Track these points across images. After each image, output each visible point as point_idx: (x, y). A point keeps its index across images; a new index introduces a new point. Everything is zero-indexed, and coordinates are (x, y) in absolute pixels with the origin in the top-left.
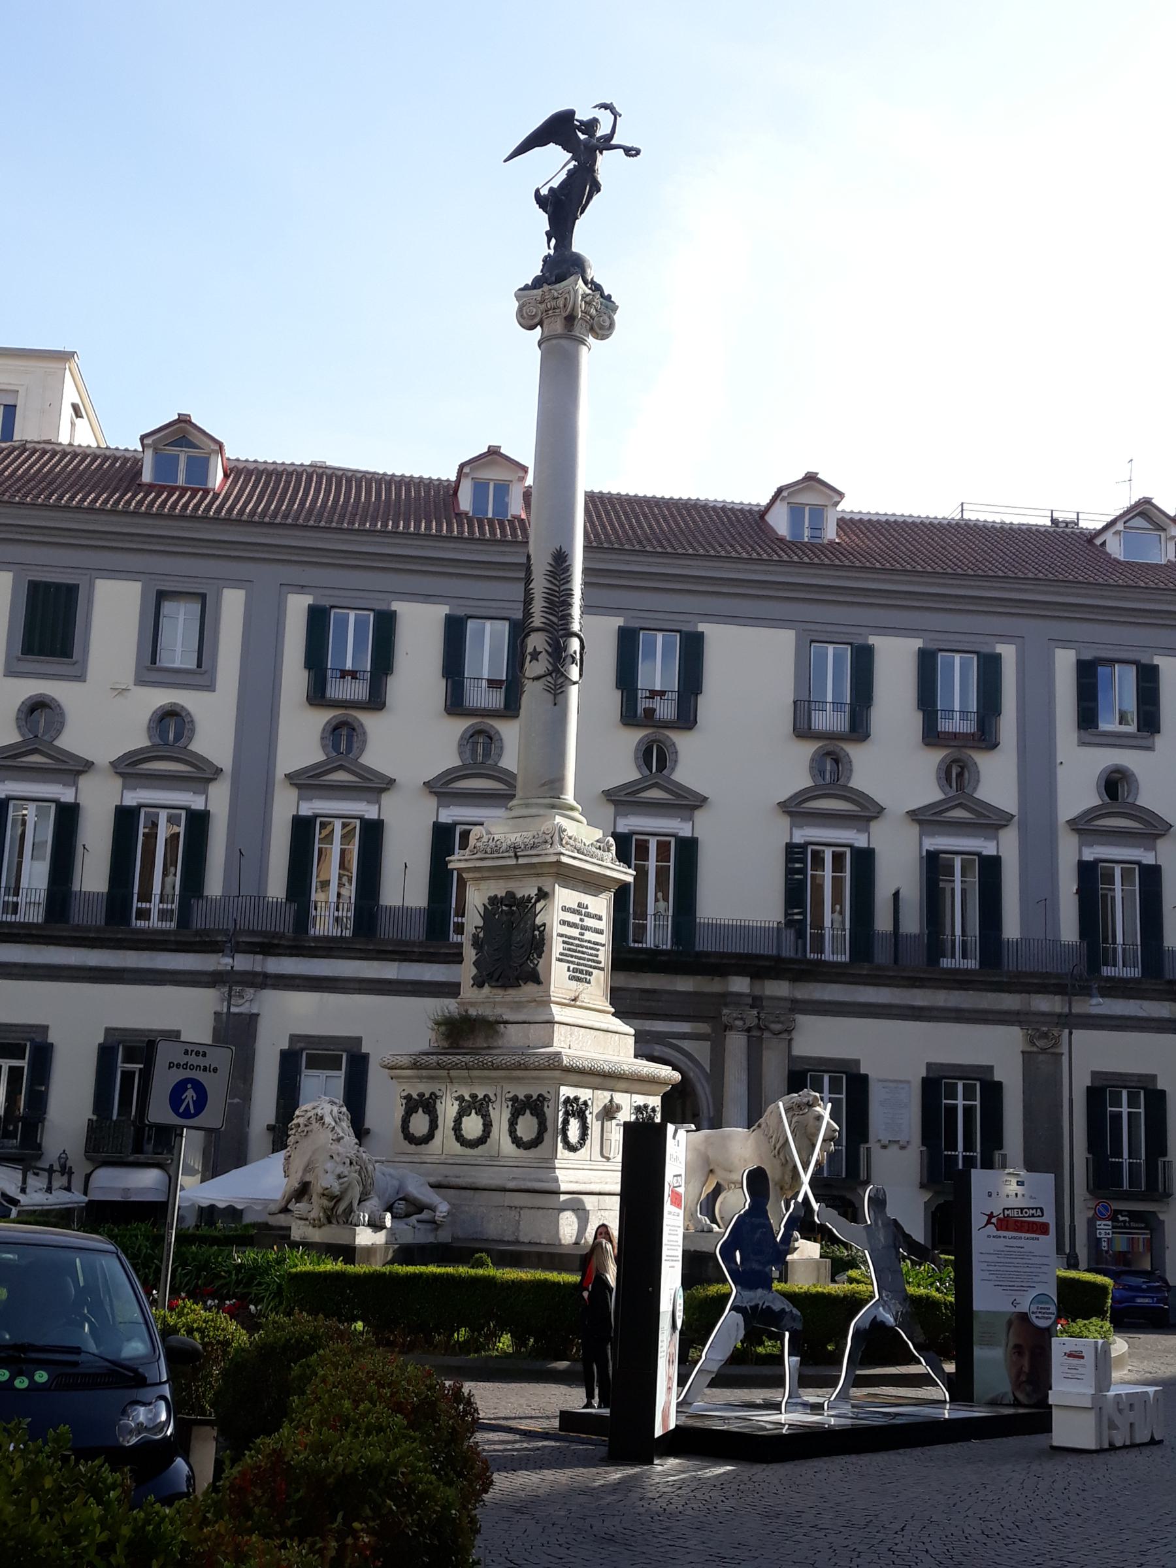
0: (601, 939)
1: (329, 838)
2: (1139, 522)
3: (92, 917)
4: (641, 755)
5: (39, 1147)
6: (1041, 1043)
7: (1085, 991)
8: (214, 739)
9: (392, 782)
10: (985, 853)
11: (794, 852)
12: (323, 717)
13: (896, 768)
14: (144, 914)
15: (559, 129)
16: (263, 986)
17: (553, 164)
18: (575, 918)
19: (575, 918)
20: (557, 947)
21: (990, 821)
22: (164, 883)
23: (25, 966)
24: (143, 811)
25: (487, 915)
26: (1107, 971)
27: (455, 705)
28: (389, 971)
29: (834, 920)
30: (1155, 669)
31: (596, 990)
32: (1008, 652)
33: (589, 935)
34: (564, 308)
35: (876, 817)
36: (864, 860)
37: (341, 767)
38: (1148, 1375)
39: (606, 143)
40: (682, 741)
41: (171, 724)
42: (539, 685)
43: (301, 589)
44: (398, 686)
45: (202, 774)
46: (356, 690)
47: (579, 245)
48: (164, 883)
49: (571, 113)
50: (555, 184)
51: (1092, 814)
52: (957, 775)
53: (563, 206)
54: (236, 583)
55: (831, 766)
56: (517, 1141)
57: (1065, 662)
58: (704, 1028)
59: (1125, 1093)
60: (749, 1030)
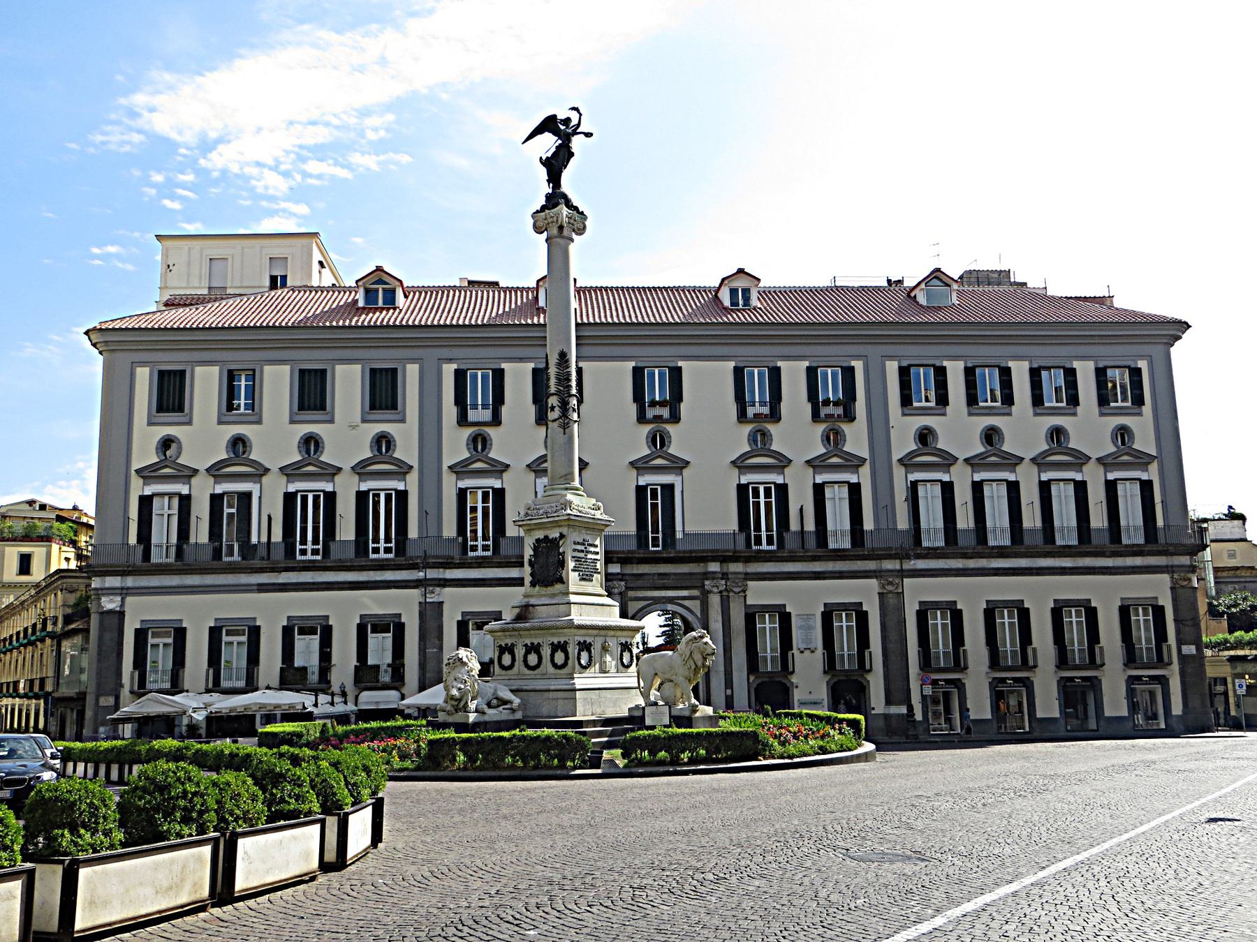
0: (598, 557)
2: (935, 282)
5: (329, 682)
6: (890, 588)
7: (908, 557)
8: (407, 451)
9: (508, 466)
11: (742, 490)
12: (467, 432)
13: (797, 434)
15: (549, 124)
16: (444, 586)
17: (548, 143)
18: (582, 548)
19: (582, 548)
20: (571, 564)
21: (854, 463)
25: (535, 549)
29: (765, 525)
30: (778, 369)
31: (596, 584)
32: (858, 365)
33: (590, 556)
34: (558, 219)
36: (782, 489)
37: (479, 460)
39: (575, 133)
41: (383, 442)
42: (556, 424)
43: (450, 360)
45: (403, 470)
46: (486, 415)
47: (566, 185)
49: (555, 116)
50: (549, 154)
51: (912, 454)
52: (833, 438)
53: (555, 165)
54: (413, 360)
55: (760, 439)
56: (555, 666)
57: (892, 368)
58: (696, 593)
59: (1073, 610)
60: (620, 593)
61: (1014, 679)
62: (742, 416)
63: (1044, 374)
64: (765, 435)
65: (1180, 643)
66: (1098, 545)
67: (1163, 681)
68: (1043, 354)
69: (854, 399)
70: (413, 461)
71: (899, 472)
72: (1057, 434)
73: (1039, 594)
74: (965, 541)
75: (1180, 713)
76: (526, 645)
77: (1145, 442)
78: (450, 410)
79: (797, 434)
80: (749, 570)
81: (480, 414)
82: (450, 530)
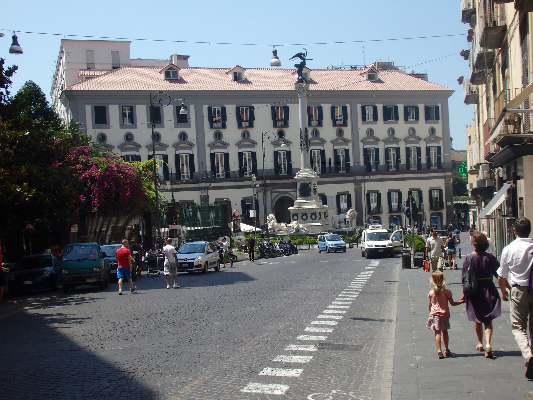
1: (218, 158)
3: (424, 167)
13: (328, 131)
14: (246, 174)
21: (346, 142)
22: (186, 170)
23: (184, 188)
26: (340, 172)
27: (334, 125)
28: (233, 184)
30: (322, 107)
32: (348, 106)
38: (370, 247)
40: (320, 129)
41: (183, 136)
43: (206, 104)
45: (191, 145)
46: (219, 125)
48: (186, 170)
52: (340, 133)
57: (359, 106)
61: (396, 216)
63: (366, 108)
64: (248, 134)
65: (447, 201)
66: (423, 169)
67: (441, 214)
69: (347, 119)
70: (195, 142)
73: (405, 186)
74: (424, 167)
77: (439, 133)
78: (207, 123)
79: (328, 131)
81: (314, 123)
82: (209, 169)
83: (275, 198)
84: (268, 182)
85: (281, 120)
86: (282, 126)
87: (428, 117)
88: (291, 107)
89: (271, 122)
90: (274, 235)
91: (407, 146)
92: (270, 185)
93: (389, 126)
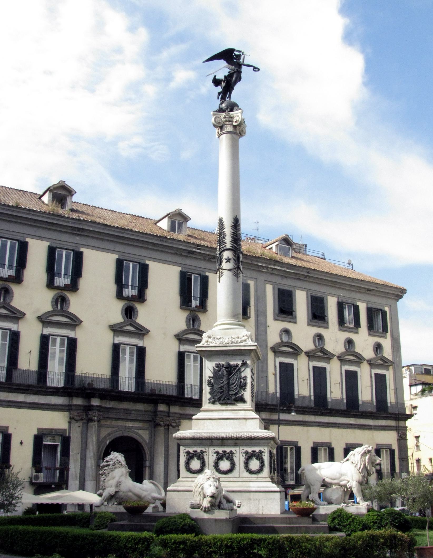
4: (124, 312)
10: (13, 329)
24: (51, 337)
28: (21, 398)
30: (147, 266)
32: (251, 283)
35: (22, 318)
44: (28, 273)
62: (120, 295)
68: (345, 295)
71: (271, 355)
72: (350, 342)
75: (127, 521)
76: (217, 453)
77: (387, 353)
80: (104, 405)
83: (105, 438)
84: (95, 402)
85: (10, 266)
86: (66, 288)
87: (371, 327)
88: (212, 277)
89: (113, 288)
90: (382, 518)
91: (182, 350)
92: (99, 408)
93: (315, 330)
